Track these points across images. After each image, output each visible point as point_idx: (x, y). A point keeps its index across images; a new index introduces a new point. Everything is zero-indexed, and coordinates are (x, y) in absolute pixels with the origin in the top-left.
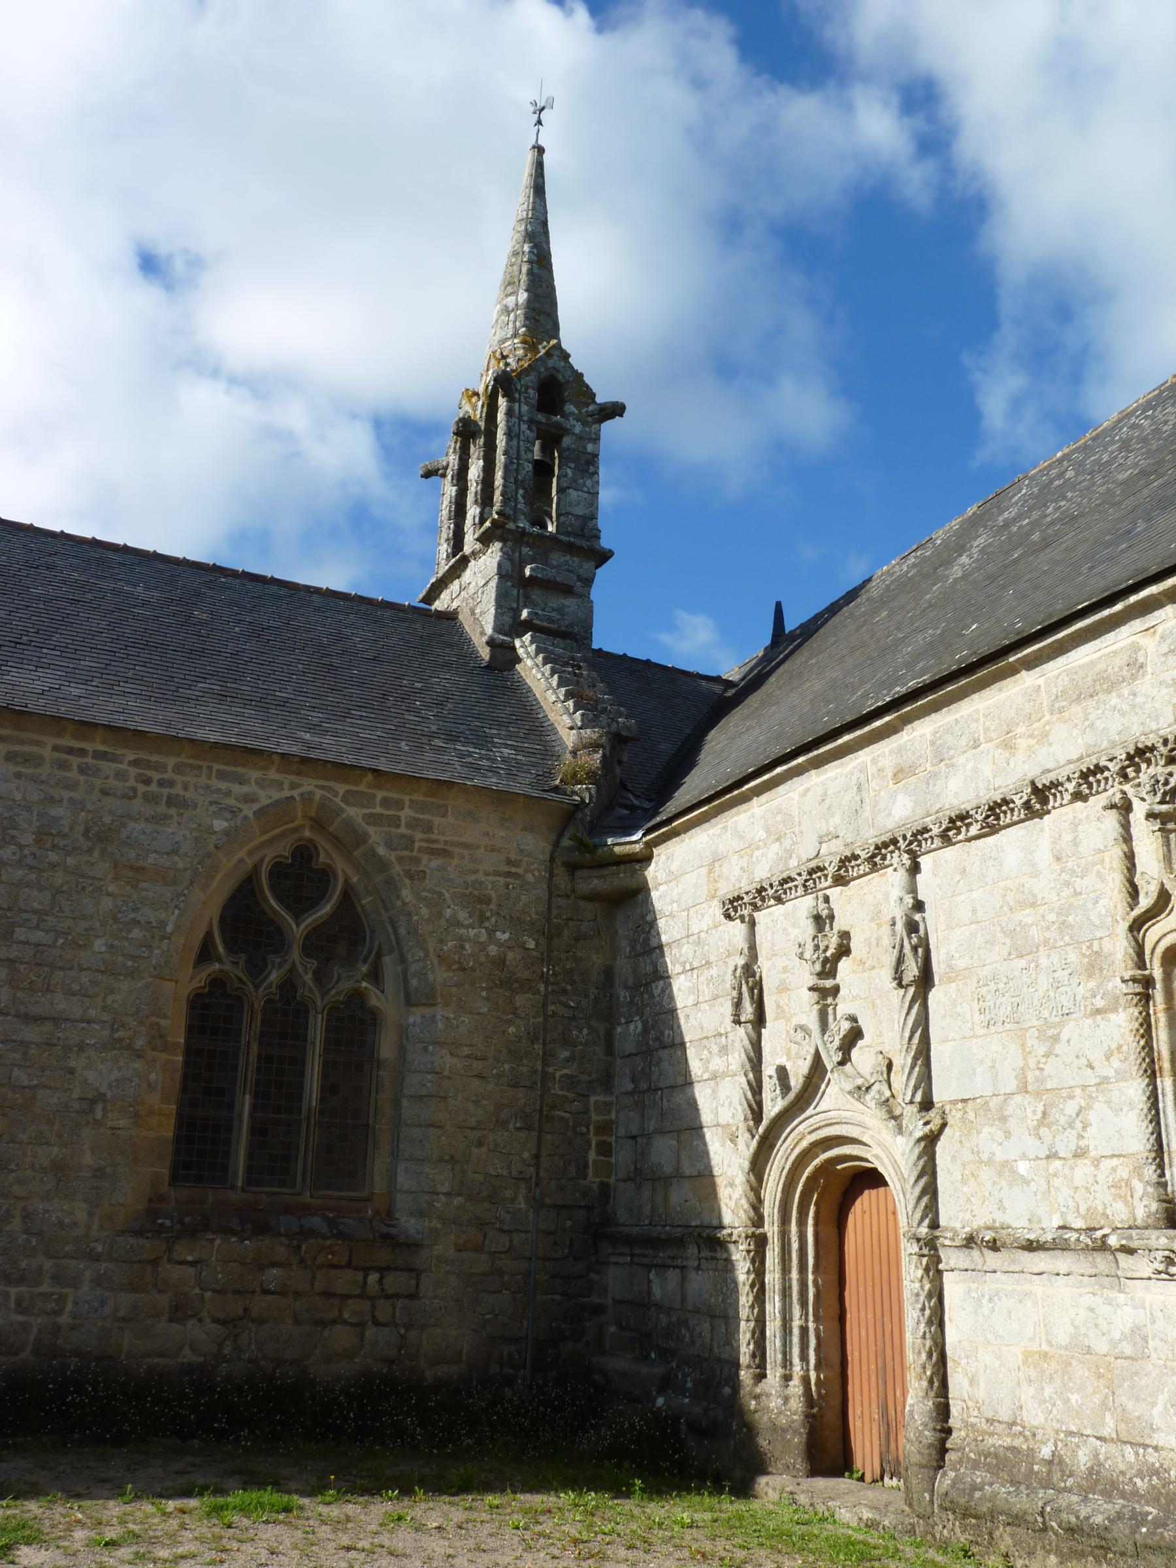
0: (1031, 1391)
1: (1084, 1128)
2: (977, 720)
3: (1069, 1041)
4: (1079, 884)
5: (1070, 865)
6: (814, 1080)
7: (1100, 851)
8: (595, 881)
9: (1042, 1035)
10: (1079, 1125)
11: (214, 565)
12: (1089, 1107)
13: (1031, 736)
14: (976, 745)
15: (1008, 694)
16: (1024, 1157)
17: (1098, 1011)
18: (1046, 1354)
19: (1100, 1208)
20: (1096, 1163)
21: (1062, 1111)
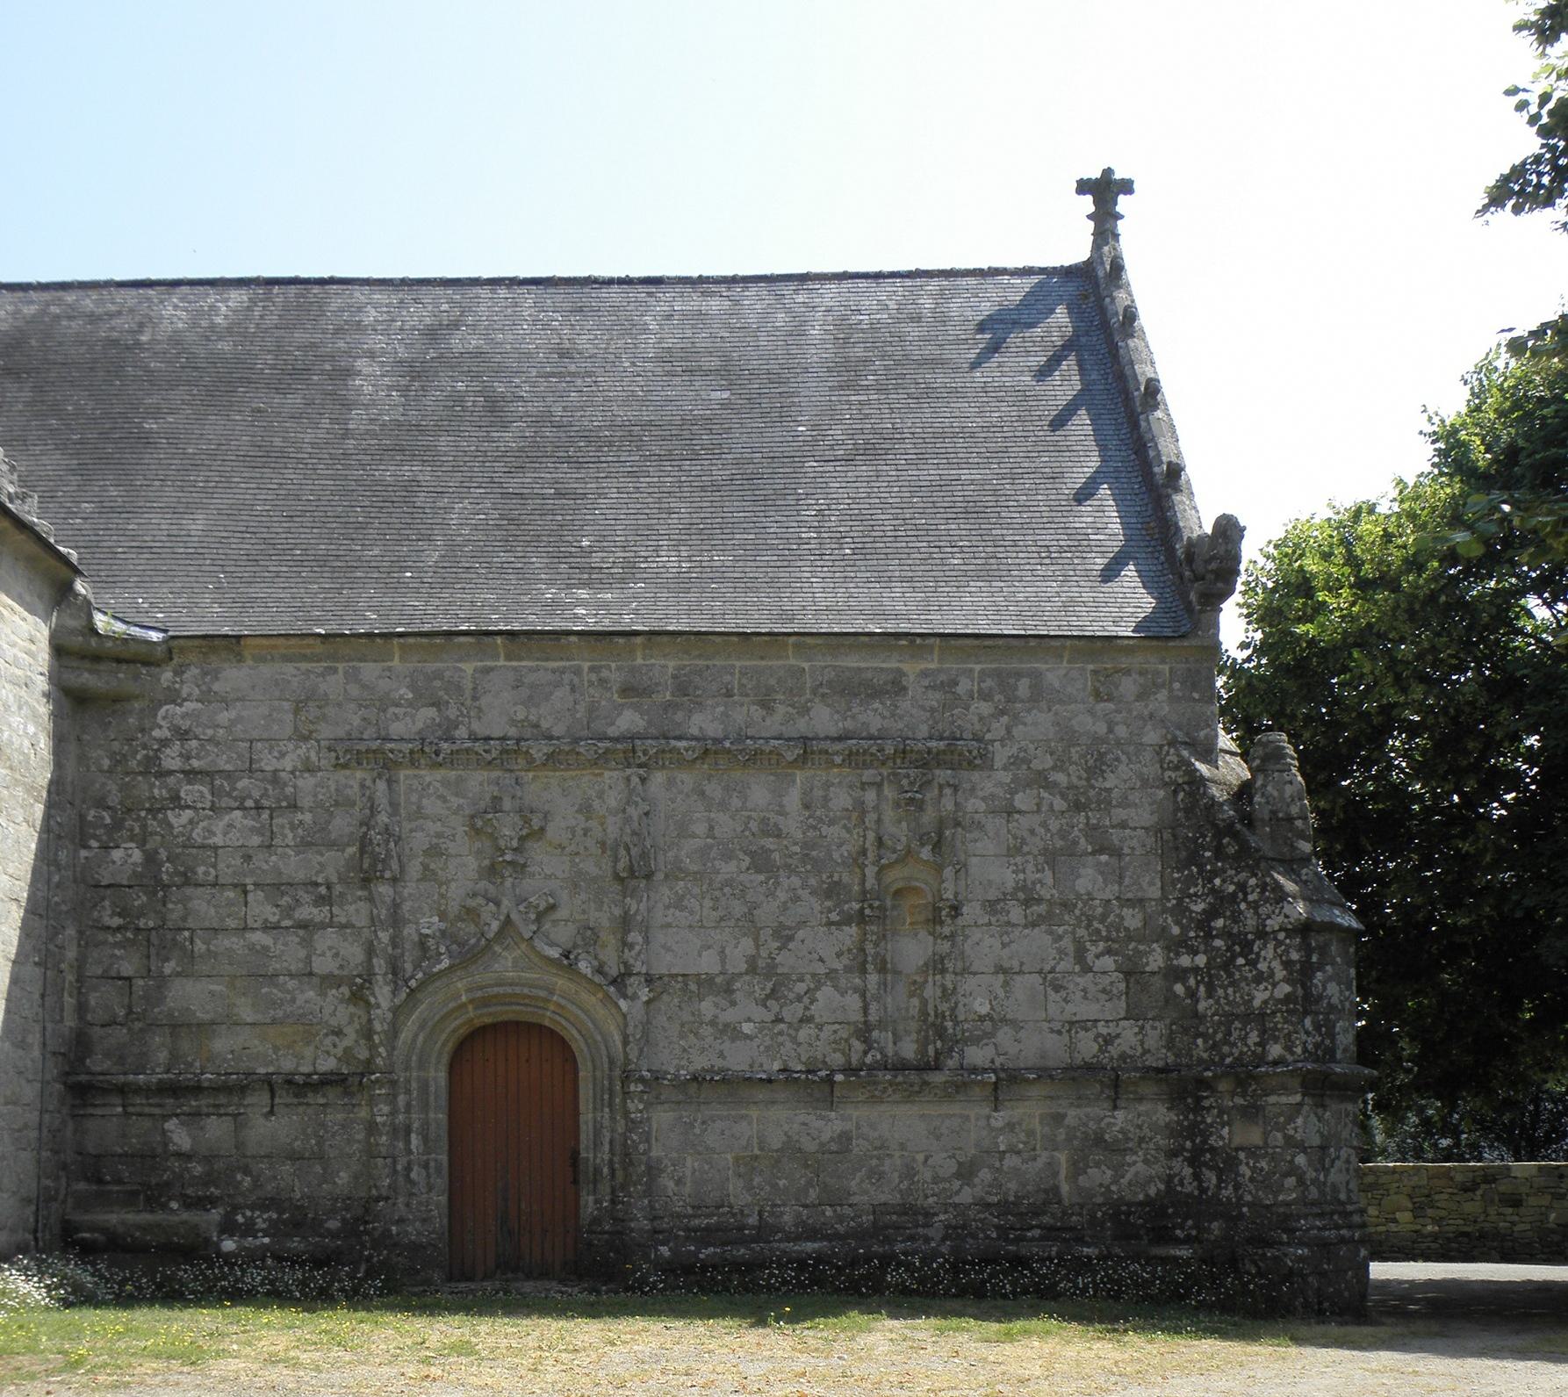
0: (741, 1183)
1: (811, 1003)
2: (732, 674)
3: (803, 941)
4: (825, 830)
5: (818, 813)
6: (523, 946)
7: (847, 810)
8: (86, 675)
9: (777, 934)
10: (806, 1000)
11: (700, 276)
12: (817, 988)
13: (792, 706)
14: (729, 694)
15: (770, 663)
16: (749, 1020)
17: (830, 924)
18: (757, 1157)
19: (820, 1057)
20: (820, 1027)
21: (790, 990)
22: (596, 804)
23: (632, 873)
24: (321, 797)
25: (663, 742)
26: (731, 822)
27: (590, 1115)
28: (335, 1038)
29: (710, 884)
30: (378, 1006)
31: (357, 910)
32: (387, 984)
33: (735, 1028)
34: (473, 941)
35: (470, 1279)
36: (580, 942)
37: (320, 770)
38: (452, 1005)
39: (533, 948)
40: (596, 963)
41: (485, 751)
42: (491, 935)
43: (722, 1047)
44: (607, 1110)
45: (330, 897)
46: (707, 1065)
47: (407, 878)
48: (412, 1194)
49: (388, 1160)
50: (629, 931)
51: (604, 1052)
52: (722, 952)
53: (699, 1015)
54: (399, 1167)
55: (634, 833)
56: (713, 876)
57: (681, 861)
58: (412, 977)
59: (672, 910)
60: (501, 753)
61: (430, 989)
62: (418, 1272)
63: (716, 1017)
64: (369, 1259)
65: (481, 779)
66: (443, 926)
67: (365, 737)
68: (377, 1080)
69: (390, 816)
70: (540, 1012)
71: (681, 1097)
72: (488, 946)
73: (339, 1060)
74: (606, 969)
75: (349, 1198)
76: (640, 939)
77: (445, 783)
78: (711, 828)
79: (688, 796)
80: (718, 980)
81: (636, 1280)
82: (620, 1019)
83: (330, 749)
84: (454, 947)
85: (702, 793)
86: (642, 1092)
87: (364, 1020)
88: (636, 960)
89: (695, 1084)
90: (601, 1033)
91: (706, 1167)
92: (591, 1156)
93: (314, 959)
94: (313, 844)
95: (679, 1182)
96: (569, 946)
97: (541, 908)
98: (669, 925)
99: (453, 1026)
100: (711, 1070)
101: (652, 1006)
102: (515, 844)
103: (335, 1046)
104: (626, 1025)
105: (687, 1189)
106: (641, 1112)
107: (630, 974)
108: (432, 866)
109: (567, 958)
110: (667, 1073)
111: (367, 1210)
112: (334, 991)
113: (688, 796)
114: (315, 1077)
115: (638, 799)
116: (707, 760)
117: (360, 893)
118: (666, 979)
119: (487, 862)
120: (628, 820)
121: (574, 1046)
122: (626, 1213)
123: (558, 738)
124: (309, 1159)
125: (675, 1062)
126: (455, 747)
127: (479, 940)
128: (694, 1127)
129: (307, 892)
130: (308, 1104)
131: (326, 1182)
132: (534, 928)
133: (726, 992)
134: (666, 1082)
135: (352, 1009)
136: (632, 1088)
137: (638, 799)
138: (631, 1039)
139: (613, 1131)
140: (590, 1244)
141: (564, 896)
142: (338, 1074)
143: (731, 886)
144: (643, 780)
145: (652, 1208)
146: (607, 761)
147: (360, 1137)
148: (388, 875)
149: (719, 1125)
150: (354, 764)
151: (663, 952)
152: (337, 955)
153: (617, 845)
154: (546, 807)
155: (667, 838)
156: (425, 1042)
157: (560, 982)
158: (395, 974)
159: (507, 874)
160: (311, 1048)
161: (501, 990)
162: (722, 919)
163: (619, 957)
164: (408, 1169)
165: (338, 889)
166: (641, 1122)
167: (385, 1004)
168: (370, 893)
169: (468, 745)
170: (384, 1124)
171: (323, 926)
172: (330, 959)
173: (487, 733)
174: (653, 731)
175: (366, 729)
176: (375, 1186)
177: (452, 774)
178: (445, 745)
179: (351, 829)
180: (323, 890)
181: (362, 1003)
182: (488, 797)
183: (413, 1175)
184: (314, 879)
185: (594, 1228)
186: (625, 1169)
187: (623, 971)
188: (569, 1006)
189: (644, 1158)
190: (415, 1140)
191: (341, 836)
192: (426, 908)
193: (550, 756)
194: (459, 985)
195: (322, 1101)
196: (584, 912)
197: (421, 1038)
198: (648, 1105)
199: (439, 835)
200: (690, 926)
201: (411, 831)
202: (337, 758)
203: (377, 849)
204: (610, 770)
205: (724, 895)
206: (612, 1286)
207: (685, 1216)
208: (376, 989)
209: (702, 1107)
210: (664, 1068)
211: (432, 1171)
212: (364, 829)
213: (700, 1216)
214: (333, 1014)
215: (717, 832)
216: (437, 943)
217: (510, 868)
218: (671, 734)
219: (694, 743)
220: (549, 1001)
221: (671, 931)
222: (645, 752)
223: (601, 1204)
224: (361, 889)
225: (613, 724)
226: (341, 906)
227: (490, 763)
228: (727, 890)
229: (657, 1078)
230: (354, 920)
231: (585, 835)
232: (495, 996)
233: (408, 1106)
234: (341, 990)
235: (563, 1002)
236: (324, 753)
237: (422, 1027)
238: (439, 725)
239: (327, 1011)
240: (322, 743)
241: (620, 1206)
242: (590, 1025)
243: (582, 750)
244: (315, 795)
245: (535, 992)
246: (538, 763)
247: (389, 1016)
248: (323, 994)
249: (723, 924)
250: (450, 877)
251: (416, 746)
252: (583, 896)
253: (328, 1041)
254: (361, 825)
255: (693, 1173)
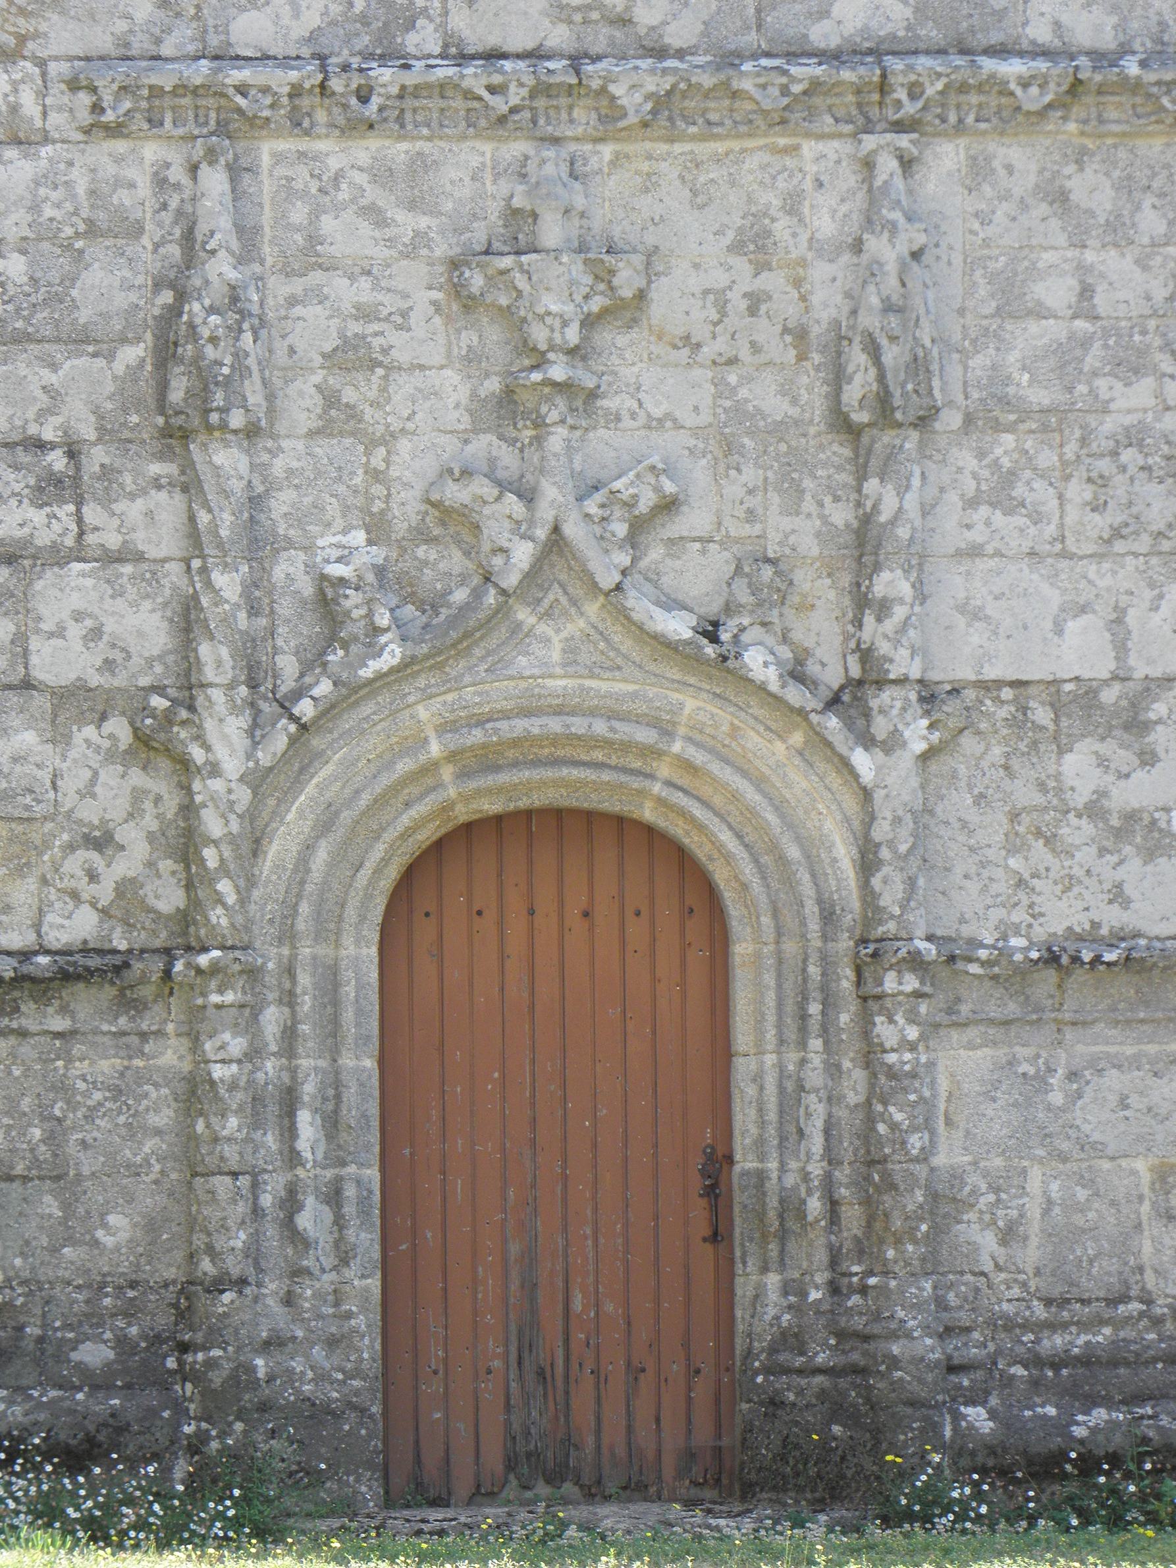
6: (593, 608)
22: (781, 228)
23: (883, 403)
24: (48, 212)
25: (959, 61)
26: (1138, 274)
27: (770, 1059)
28: (94, 855)
29: (1084, 441)
30: (214, 770)
31: (149, 514)
32: (235, 710)
33: (1154, 822)
34: (460, 596)
35: (437, 1502)
36: (743, 596)
37: (46, 139)
38: (404, 766)
39: (624, 615)
40: (785, 653)
41: (492, 89)
42: (511, 580)
43: (1121, 874)
44: (816, 1044)
45: (77, 479)
46: (1080, 923)
47: (281, 427)
48: (298, 1273)
49: (244, 1181)
50: (877, 568)
51: (807, 889)
52: (1118, 621)
53: (1059, 791)
54: (266, 1200)
55: (889, 308)
56: (1092, 419)
57: (1007, 381)
58: (298, 694)
59: (984, 511)
60: (533, 95)
61: (348, 722)
62: (318, 1479)
63: (1102, 794)
64: (195, 1447)
65: (475, 161)
66: (378, 554)
67: (166, 50)
68: (215, 969)
69: (241, 261)
70: (636, 783)
71: (1013, 1008)
72: (502, 610)
73: (104, 912)
74: (812, 668)
75: (133, 1285)
76: (905, 588)
77: (382, 174)
78: (1086, 292)
79: (1024, 206)
80: (1109, 696)
81: (915, 1496)
82: (851, 804)
83: (74, 85)
84: (409, 610)
85: (1061, 199)
86: (918, 995)
87: (171, 805)
88: (897, 643)
89: (1051, 975)
90: (798, 839)
91: (1082, 1194)
92: (773, 1165)
93: (34, 643)
94: (28, 338)
95: (1009, 1235)
96: (713, 608)
97: (643, 507)
98: (974, 552)
99: (405, 820)
100: (1091, 936)
101: (933, 767)
102: (573, 335)
103: (93, 877)
104: (870, 818)
105: (1031, 1254)
106: (913, 1047)
107: (881, 683)
108: (349, 395)
109: (714, 639)
110: (977, 944)
111: (183, 1315)
112: (90, 731)
113: (1024, 206)
114: (43, 960)
115: (897, 216)
116: (1077, 111)
117: (156, 468)
118: (970, 694)
119: (493, 385)
120: (873, 272)
121: (720, 875)
122: (877, 1317)
123: (680, 54)
124: (25, 1179)
125: (996, 914)
126: (411, 79)
127: (477, 594)
128: (1046, 1088)
129: (16, 467)
130: (23, 1034)
131: (70, 1241)
132: (623, 558)
133: (1127, 727)
134: (974, 969)
135: (137, 777)
136: (890, 983)
137: (897, 216)
138: (885, 853)
139: (832, 1099)
140: (775, 1403)
141: (700, 474)
142: (100, 952)
143: (1140, 445)
144: (907, 164)
145: (941, 1304)
146: (812, 114)
147: (163, 1118)
148: (237, 419)
149: (1114, 1080)
150: (139, 122)
151: (961, 621)
152: (96, 633)
153: (839, 339)
154: (651, 239)
155: (969, 319)
156: (332, 865)
157: (690, 704)
158: (253, 685)
159: (553, 416)
160: (32, 883)
161: (534, 726)
162: (1117, 533)
163: (847, 637)
164: (291, 1202)
165: (97, 457)
166: (914, 1075)
167: (233, 766)
168: (188, 466)
169: (445, 72)
170: (233, 1086)
171: (58, 557)
172: (78, 645)
173: (493, 40)
174: (931, 33)
175: (168, 31)
176: (210, 1250)
177: (400, 151)
178: (385, 76)
179: (133, 297)
180: (57, 461)
181: (164, 764)
182: (494, 210)
183: (304, 1221)
184: (33, 429)
185: (782, 1357)
186: (867, 1202)
187: (855, 672)
188: (715, 767)
189: (921, 1170)
190: (307, 1125)
191: (105, 316)
192: (333, 508)
193: (662, 103)
194: (422, 713)
195: (60, 1024)
196: (751, 516)
197: (322, 855)
198: (932, 1028)
199: (365, 313)
200: (1032, 554)
201: (292, 301)
202: (97, 108)
203: (210, 352)
204: (821, 137)
205: (1123, 469)
206: (840, 1513)
207: (1026, 1326)
208: (209, 725)
209: (1069, 1034)
210: (966, 931)
211: (349, 1210)
212: (167, 297)
213: (1065, 1326)
214: (89, 792)
215: (1102, 302)
216: (369, 602)
217: (561, 403)
218: (982, 40)
219: (1042, 65)
220: (658, 754)
221: (982, 565)
222: (915, 90)
223: (804, 1294)
224: (161, 456)
225: (824, 14)
226: (106, 502)
227: (502, 120)
228: (1128, 456)
229: (952, 959)
230: (141, 540)
231: (753, 311)
232: (515, 743)
233: (290, 1034)
234: (110, 726)
235: (699, 757)
236: (58, 95)
237: (324, 827)
238: (364, 20)
239: (71, 784)
240: (53, 68)
241: (855, 1300)
242: (771, 817)
243: (747, 85)
244: (35, 208)
245: (625, 730)
246: (632, 119)
247: (244, 795)
248: (59, 738)
249: (1119, 546)
250: (396, 425)
251: (310, 74)
252: (750, 475)
253: (74, 864)
254: (157, 286)
255: (1046, 1212)
